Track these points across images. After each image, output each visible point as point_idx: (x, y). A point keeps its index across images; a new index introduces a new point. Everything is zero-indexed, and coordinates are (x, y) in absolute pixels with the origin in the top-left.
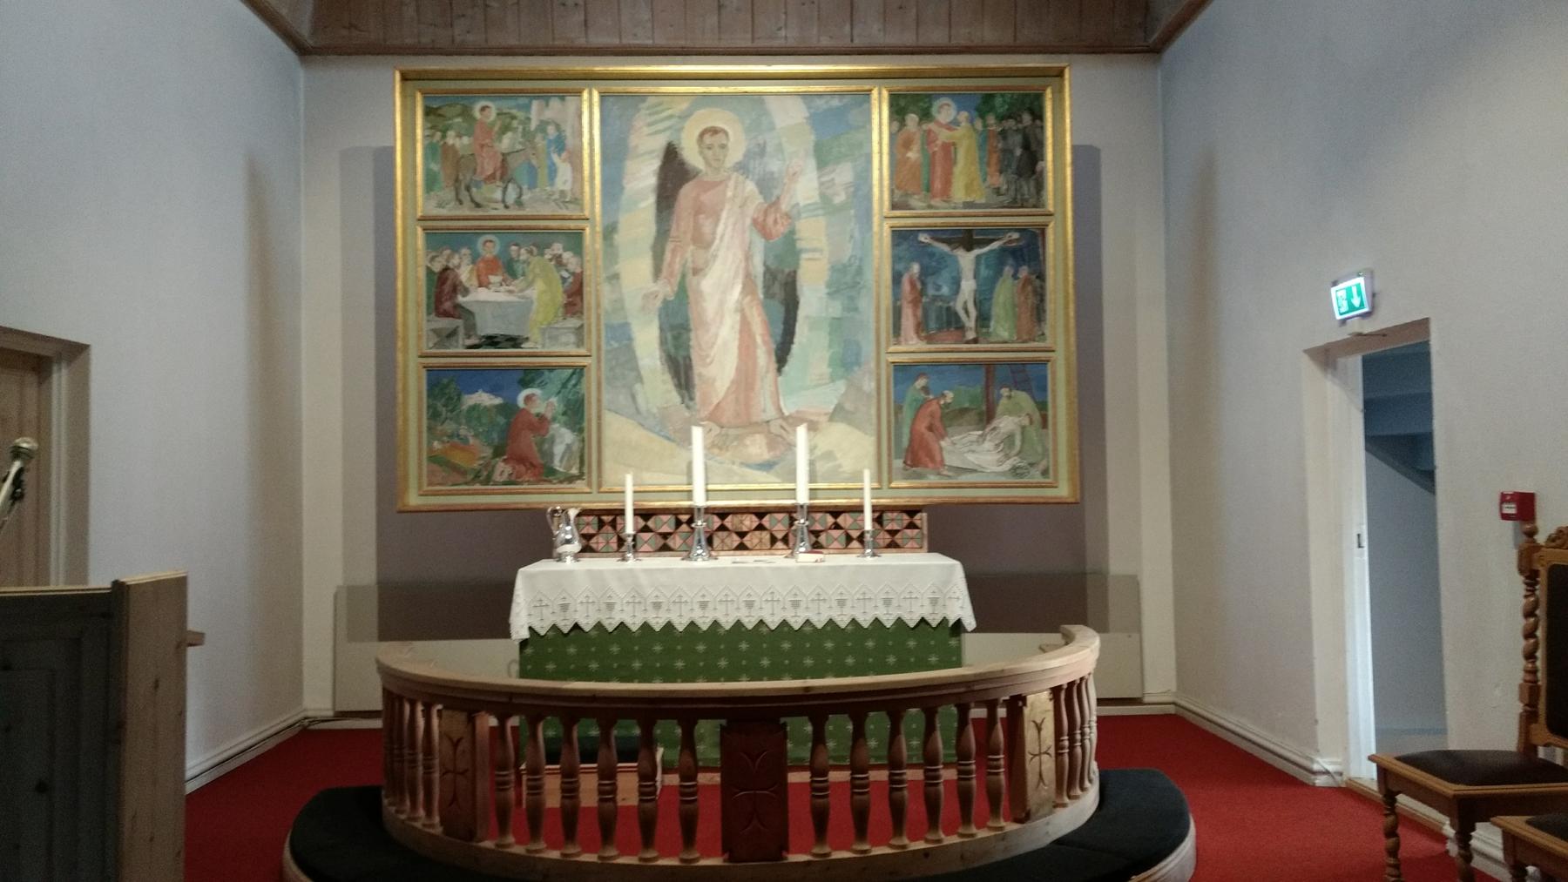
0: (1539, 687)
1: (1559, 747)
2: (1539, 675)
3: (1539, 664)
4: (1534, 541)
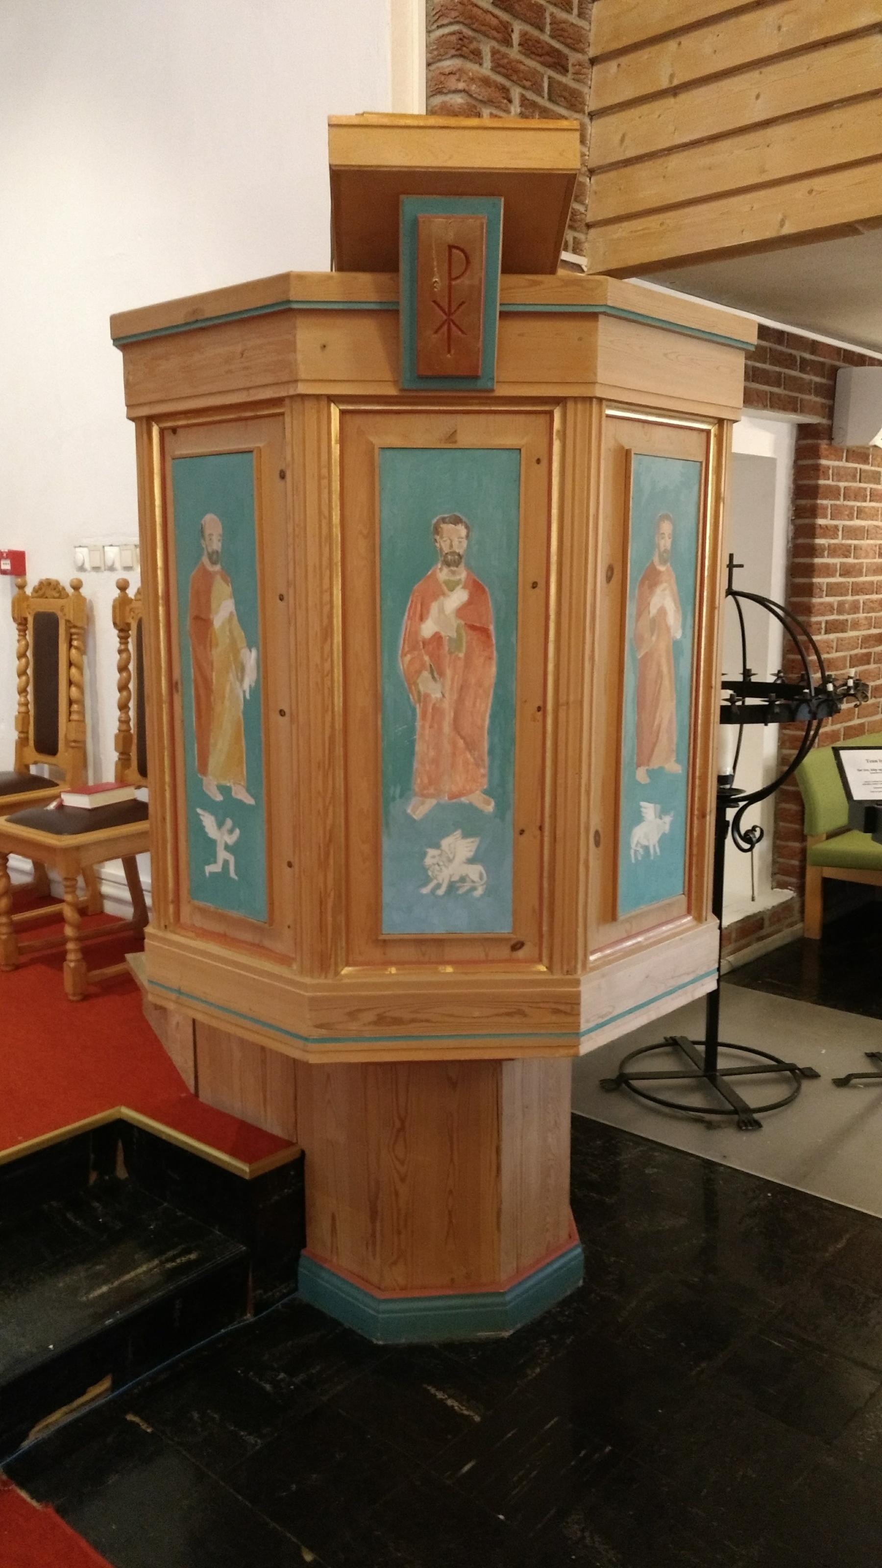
0: (131, 735)
1: (46, 763)
2: (132, 724)
3: (30, 697)
4: (126, 595)
